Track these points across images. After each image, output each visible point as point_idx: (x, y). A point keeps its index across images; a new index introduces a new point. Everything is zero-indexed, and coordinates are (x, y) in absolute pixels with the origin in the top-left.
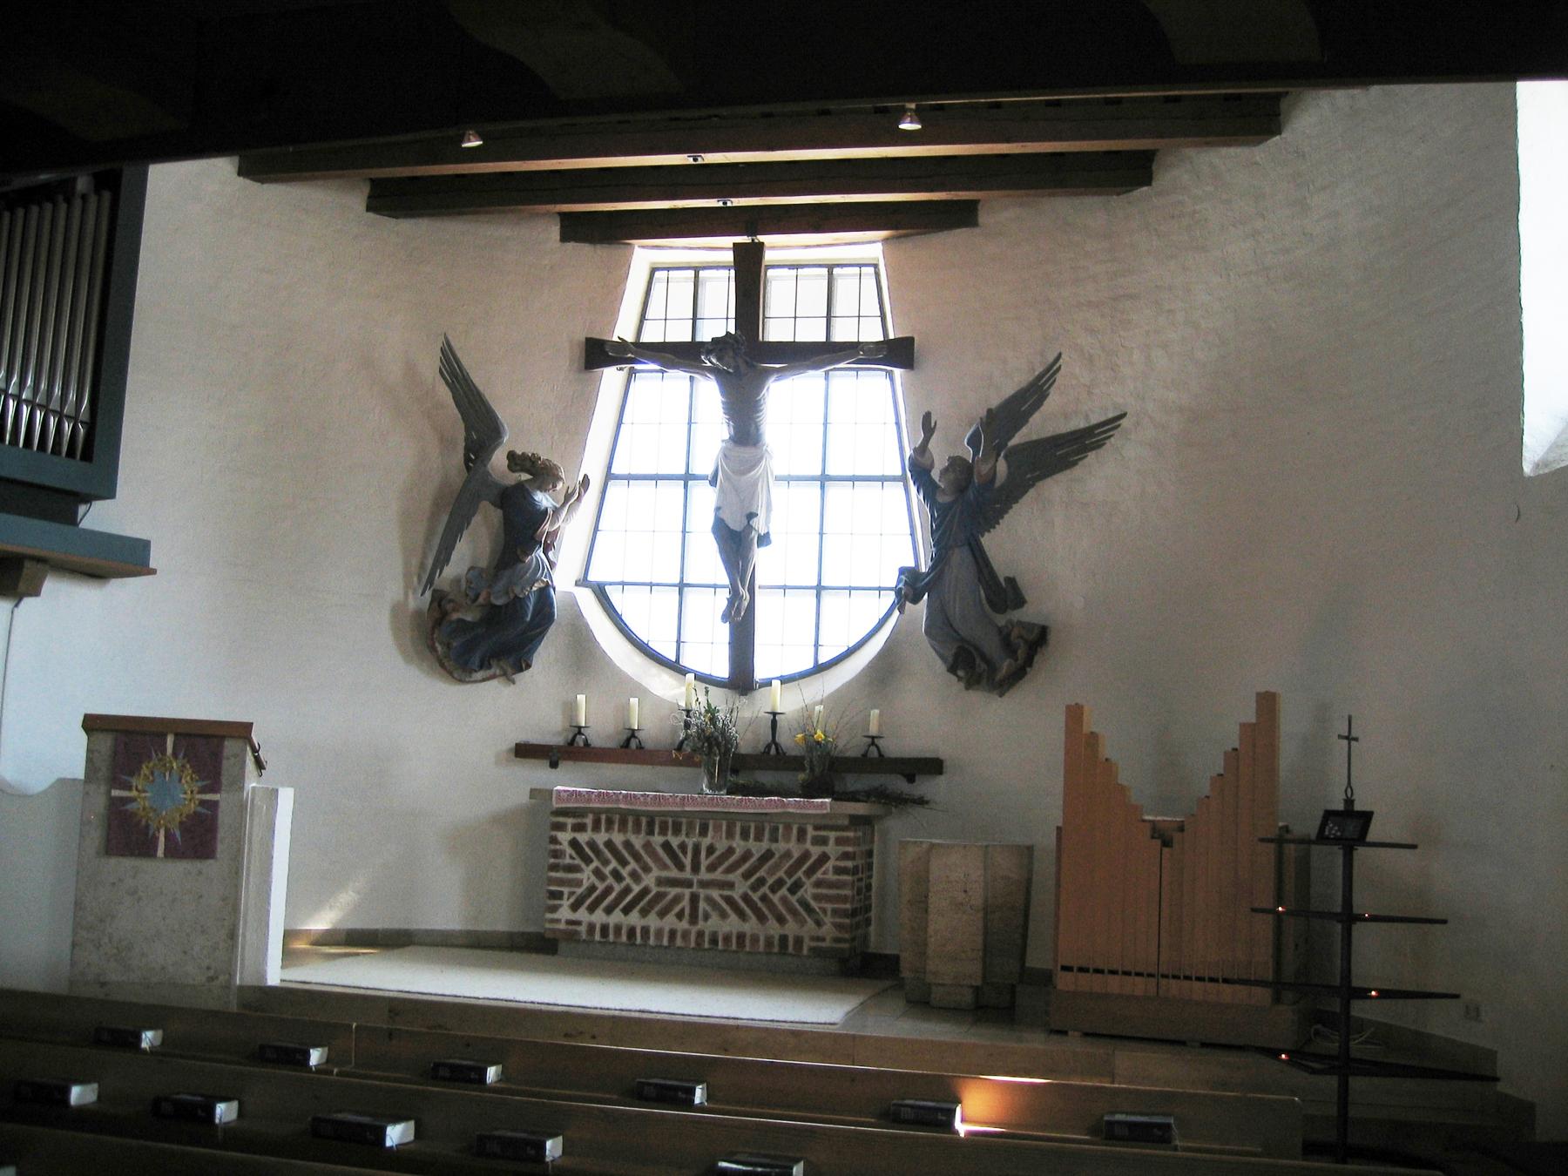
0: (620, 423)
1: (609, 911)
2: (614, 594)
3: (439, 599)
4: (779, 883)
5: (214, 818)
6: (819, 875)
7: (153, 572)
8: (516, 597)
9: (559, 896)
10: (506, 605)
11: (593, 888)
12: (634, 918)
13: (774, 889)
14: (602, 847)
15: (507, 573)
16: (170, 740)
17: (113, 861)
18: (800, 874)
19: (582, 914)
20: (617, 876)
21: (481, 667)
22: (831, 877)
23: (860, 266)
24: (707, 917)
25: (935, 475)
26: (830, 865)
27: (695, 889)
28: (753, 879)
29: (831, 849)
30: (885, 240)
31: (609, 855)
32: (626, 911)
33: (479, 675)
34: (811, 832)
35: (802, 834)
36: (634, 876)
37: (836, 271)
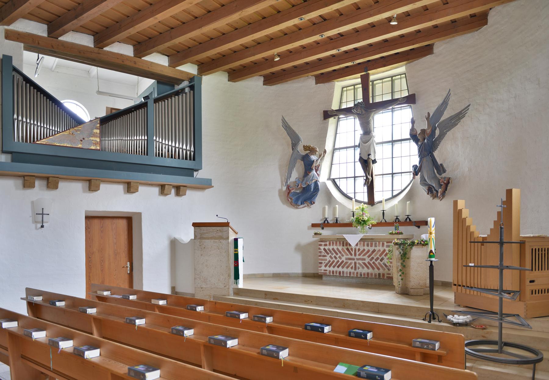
0: (336, 133)
1: (334, 267)
3: (288, 187)
7: (213, 187)
11: (330, 261)
12: (340, 269)
13: (376, 260)
15: (306, 178)
18: (383, 256)
19: (327, 268)
20: (336, 258)
21: (302, 204)
23: (401, 75)
24: (359, 268)
27: (355, 261)
30: (406, 64)
32: (338, 267)
33: (302, 206)
35: (383, 244)
36: (340, 257)
37: (394, 78)
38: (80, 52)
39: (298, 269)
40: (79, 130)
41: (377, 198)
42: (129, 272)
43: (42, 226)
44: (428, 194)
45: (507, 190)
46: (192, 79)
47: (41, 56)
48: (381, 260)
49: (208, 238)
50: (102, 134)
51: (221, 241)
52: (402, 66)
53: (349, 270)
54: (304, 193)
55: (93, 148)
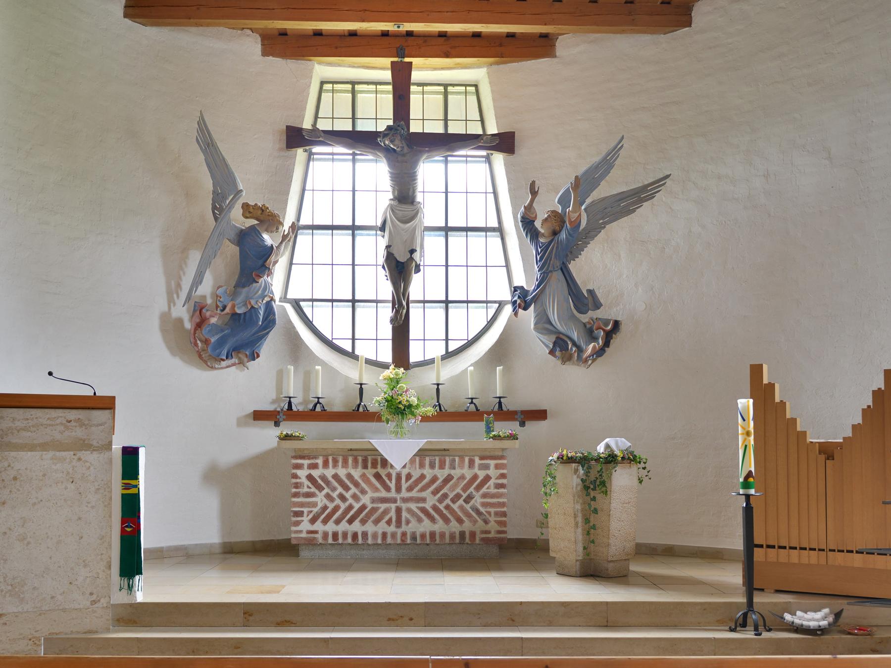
1: (338, 522)
2: (306, 307)
4: (458, 496)
6: (484, 490)
8: (252, 307)
9: (301, 514)
10: (245, 313)
11: (325, 508)
12: (356, 526)
13: (454, 501)
14: (330, 479)
18: (472, 489)
19: (318, 526)
20: (343, 498)
22: (493, 490)
23: (466, 85)
24: (408, 522)
25: (538, 224)
26: (491, 483)
28: (439, 495)
29: (492, 472)
31: (336, 484)
32: (350, 522)
34: (477, 461)
35: (471, 463)
36: (355, 497)
37: (450, 89)
39: (210, 534)
41: (415, 355)
44: (552, 352)
48: (467, 501)
49: (32, 448)
51: (85, 455)
52: (479, 66)
53: (382, 527)
54: (233, 327)
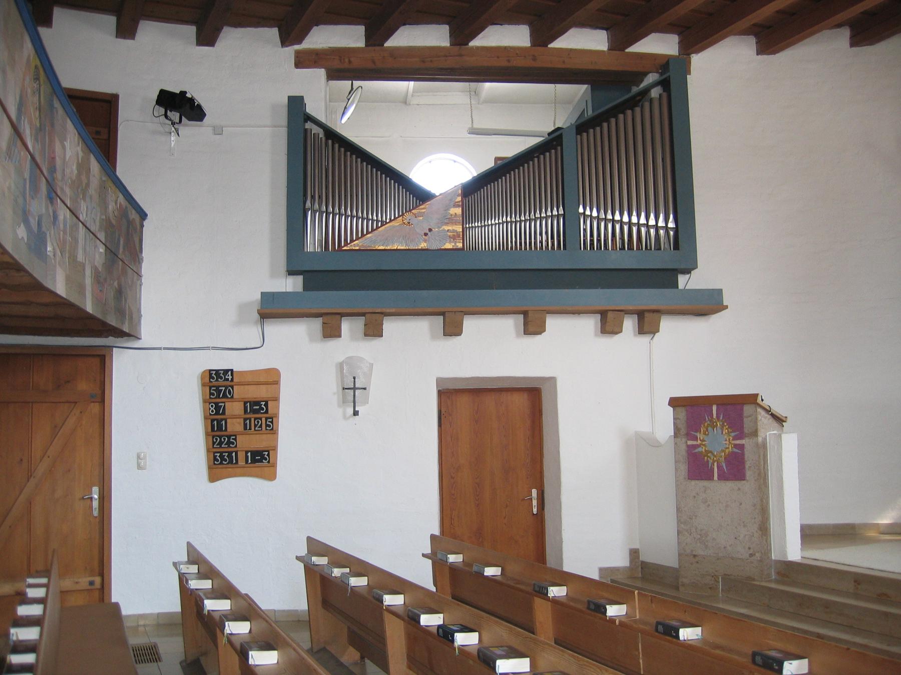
5: (743, 454)
7: (726, 307)
16: (714, 408)
17: (693, 482)
38: (424, 62)
40: (422, 214)
42: (535, 511)
43: (356, 413)
45: (261, 460)
46: (664, 65)
47: (357, 83)
50: (468, 216)
55: (449, 246)
